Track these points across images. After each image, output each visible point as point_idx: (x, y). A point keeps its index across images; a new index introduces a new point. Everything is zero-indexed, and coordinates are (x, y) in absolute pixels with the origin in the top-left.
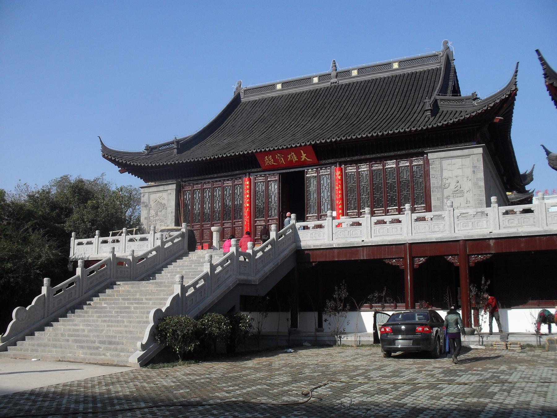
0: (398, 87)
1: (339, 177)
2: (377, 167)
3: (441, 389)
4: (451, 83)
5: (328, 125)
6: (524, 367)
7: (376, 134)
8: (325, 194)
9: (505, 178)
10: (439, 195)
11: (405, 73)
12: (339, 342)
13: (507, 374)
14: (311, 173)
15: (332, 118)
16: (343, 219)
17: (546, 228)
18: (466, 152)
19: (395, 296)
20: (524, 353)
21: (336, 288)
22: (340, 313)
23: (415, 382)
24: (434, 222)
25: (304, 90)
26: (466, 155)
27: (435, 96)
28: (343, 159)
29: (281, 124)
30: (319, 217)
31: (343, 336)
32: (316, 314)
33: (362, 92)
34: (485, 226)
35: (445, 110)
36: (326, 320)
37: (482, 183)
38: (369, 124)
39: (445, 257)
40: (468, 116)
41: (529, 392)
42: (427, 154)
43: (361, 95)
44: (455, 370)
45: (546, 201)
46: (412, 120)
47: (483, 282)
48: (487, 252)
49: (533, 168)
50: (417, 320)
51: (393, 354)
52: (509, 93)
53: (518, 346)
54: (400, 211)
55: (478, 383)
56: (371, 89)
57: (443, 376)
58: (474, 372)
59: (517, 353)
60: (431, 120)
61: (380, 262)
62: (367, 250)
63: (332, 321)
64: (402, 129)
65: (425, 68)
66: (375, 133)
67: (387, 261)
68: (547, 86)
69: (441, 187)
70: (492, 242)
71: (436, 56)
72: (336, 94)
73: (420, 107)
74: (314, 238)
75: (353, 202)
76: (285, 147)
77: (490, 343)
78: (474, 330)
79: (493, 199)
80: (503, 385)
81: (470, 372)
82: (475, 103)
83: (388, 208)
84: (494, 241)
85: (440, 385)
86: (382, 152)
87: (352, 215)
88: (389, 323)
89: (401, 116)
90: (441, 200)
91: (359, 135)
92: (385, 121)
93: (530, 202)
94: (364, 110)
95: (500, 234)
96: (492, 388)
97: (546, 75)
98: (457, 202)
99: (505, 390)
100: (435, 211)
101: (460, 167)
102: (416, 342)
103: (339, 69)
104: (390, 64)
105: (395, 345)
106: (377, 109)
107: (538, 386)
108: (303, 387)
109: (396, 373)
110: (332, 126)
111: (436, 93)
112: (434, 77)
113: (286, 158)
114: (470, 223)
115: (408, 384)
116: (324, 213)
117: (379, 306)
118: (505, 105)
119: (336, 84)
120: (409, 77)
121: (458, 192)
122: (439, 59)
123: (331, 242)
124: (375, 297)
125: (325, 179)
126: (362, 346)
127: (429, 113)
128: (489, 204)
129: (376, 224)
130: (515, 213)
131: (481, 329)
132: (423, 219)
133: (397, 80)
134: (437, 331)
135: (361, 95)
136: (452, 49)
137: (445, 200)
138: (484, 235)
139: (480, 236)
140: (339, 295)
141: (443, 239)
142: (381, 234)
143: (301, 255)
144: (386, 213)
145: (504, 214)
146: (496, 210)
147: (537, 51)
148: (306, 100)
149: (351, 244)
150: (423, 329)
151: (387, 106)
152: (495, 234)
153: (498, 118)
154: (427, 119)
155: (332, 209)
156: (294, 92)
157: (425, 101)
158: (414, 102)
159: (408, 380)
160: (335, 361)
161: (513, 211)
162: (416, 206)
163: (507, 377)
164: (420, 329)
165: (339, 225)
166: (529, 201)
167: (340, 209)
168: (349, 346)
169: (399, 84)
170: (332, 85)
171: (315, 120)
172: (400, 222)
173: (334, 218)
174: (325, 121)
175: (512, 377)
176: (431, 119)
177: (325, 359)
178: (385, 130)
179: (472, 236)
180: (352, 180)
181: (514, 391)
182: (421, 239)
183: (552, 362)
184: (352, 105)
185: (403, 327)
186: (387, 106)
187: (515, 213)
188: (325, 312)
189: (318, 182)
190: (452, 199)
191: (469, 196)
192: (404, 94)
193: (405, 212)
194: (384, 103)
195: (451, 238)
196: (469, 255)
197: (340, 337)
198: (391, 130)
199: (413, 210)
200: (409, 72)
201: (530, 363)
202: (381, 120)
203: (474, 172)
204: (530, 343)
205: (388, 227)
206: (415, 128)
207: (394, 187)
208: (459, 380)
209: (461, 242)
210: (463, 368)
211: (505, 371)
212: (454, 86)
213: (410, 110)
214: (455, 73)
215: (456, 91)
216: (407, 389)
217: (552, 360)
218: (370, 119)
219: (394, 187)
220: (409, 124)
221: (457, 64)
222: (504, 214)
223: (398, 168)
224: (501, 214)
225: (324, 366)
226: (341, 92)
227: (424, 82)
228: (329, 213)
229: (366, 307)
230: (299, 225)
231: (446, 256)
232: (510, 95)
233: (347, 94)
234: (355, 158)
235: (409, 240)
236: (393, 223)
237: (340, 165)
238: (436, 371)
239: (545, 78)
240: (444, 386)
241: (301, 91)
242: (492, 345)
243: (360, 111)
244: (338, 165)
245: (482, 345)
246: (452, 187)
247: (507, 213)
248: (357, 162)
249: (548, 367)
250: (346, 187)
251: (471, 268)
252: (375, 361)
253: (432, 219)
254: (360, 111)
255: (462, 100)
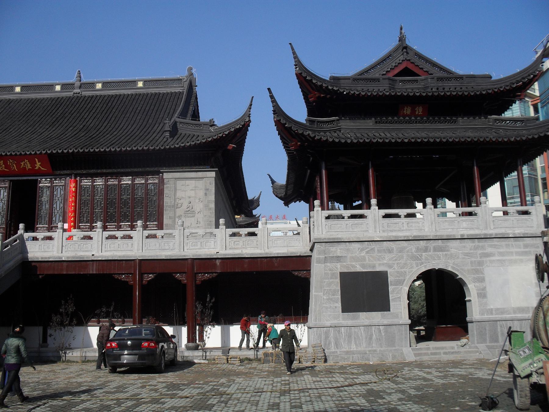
0: (141, 106)
1: (73, 189)
2: (113, 182)
3: (164, 403)
4: (191, 108)
5: (67, 136)
6: (241, 379)
7: (114, 149)
8: (58, 205)
9: (234, 202)
10: (172, 214)
11: (149, 92)
12: (64, 358)
13: (225, 387)
14: (44, 183)
15: (71, 128)
16: (74, 231)
17: (267, 251)
18: (200, 174)
19: (125, 312)
20: (242, 366)
21: (63, 302)
22: (66, 328)
23: (138, 397)
24: (165, 240)
25: (45, 97)
26: (200, 178)
27: (175, 118)
28: (79, 172)
29: (17, 129)
30: (50, 229)
31: (68, 352)
32: (41, 329)
33: (105, 106)
34: (213, 246)
35: (184, 133)
36: (51, 335)
37: (213, 206)
38: (108, 139)
39: (174, 275)
40: (204, 141)
41: (243, 402)
42: (162, 173)
43: (103, 108)
44: (178, 384)
45: (269, 226)
46: (151, 139)
47: (208, 300)
48: (213, 271)
49: (260, 194)
50: (144, 335)
51: (118, 370)
52: (243, 124)
53: (238, 359)
54: (133, 227)
55: (199, 396)
56: (114, 104)
57: (167, 391)
58: (196, 386)
59: (236, 366)
60: (169, 141)
61: (110, 276)
62: (96, 265)
63: (57, 336)
64: (140, 147)
65: (169, 90)
66: (113, 148)
67: (116, 277)
68: (275, 121)
69: (173, 206)
70: (218, 262)
71: (179, 80)
72: (78, 106)
73: (160, 128)
74: (43, 250)
75: (86, 215)
76: (18, 154)
77: (213, 357)
78: (198, 346)
79: (222, 221)
80: (221, 397)
81: (192, 385)
82: (212, 129)
83: (121, 224)
84: (220, 261)
85: (163, 400)
86: (119, 168)
87: (84, 228)
88: (115, 338)
89: (141, 134)
90: (173, 219)
91: (97, 148)
92: (124, 137)
93: (256, 226)
94: (105, 124)
95: (226, 255)
96: (212, 400)
97: (275, 112)
98: (188, 221)
99: (222, 402)
100: (167, 229)
101: (194, 189)
102: (141, 357)
103: (84, 80)
104: (135, 82)
105: (120, 360)
106: (118, 125)
107: (252, 396)
108: (20, 408)
109: (120, 389)
110: (70, 136)
111: (176, 115)
112: (176, 100)
113: (18, 165)
114: (199, 243)
115: (131, 400)
116: (55, 225)
117: (106, 321)
118: (238, 134)
119: (79, 95)
120: (153, 97)
121: (190, 212)
122: (182, 83)
123: (60, 255)
124: (103, 312)
125: (59, 189)
126: (88, 361)
127: (167, 134)
128: (217, 226)
129: (107, 238)
130: (241, 235)
131: (205, 344)
132: (154, 236)
133: (140, 98)
134: (163, 346)
135: (103, 108)
136: (196, 75)
137: (177, 219)
138: (212, 255)
139: (208, 255)
140: (66, 309)
141: (172, 256)
142: (112, 249)
143: (28, 267)
144: (119, 228)
145: (231, 236)
146: (223, 232)
147: (269, 89)
148: (45, 108)
149: (80, 258)
150: (149, 345)
151: (127, 123)
152: (221, 255)
153: (231, 146)
154: (165, 139)
155: (64, 222)
156: (33, 97)
157: (165, 122)
158: (154, 122)
159: (131, 396)
160: (57, 378)
161: (51, 237)
162: (148, 223)
163: (226, 389)
164: (146, 344)
165: (70, 238)
166: (255, 225)
167: (72, 222)
168: (74, 362)
169: (142, 103)
170: (75, 95)
171: (54, 129)
172: (131, 238)
173: (64, 230)
174: (64, 131)
175: (230, 389)
176: (170, 140)
177: (47, 376)
178: (123, 145)
179: (200, 255)
180: (86, 193)
181: (231, 402)
182: (151, 256)
183: (265, 373)
184: (92, 118)
185: (129, 342)
186: (127, 123)
187: (241, 235)
188: (51, 326)
189: (51, 192)
190: (183, 219)
191: (200, 217)
192: (145, 113)
193: (137, 229)
194: (125, 119)
195: (180, 256)
196: (196, 273)
197: (65, 353)
198: (129, 147)
199: (145, 227)
200: (153, 92)
201: (247, 375)
202: (121, 136)
203: (206, 194)
204: (248, 357)
205: (120, 243)
206: (153, 148)
207: (128, 203)
208: (181, 393)
209: (189, 261)
210: (186, 382)
211: (224, 383)
212: (194, 111)
213: (150, 129)
214: (197, 98)
215: (196, 116)
216: (129, 405)
217: (266, 371)
218: (110, 133)
219: (128, 203)
220: (148, 142)
221: (199, 91)
222: (231, 236)
223: (133, 185)
224: (227, 236)
225: (45, 383)
226: (83, 103)
227: (166, 104)
228: (60, 225)
229: (94, 322)
230: (27, 235)
231: (175, 273)
232: (243, 126)
233: (88, 106)
234: (92, 171)
235: (139, 257)
236: (125, 238)
237: (76, 177)
238: (160, 386)
239: (274, 114)
240: (166, 401)
241: (42, 97)
242: (214, 360)
243: (100, 125)
244: (73, 177)
245: (205, 359)
246: (185, 207)
247: (234, 235)
248: (93, 176)
249: (262, 378)
250: (80, 200)
251: (197, 286)
252: (100, 377)
253: (162, 237)
254: (100, 125)
255: (200, 125)
